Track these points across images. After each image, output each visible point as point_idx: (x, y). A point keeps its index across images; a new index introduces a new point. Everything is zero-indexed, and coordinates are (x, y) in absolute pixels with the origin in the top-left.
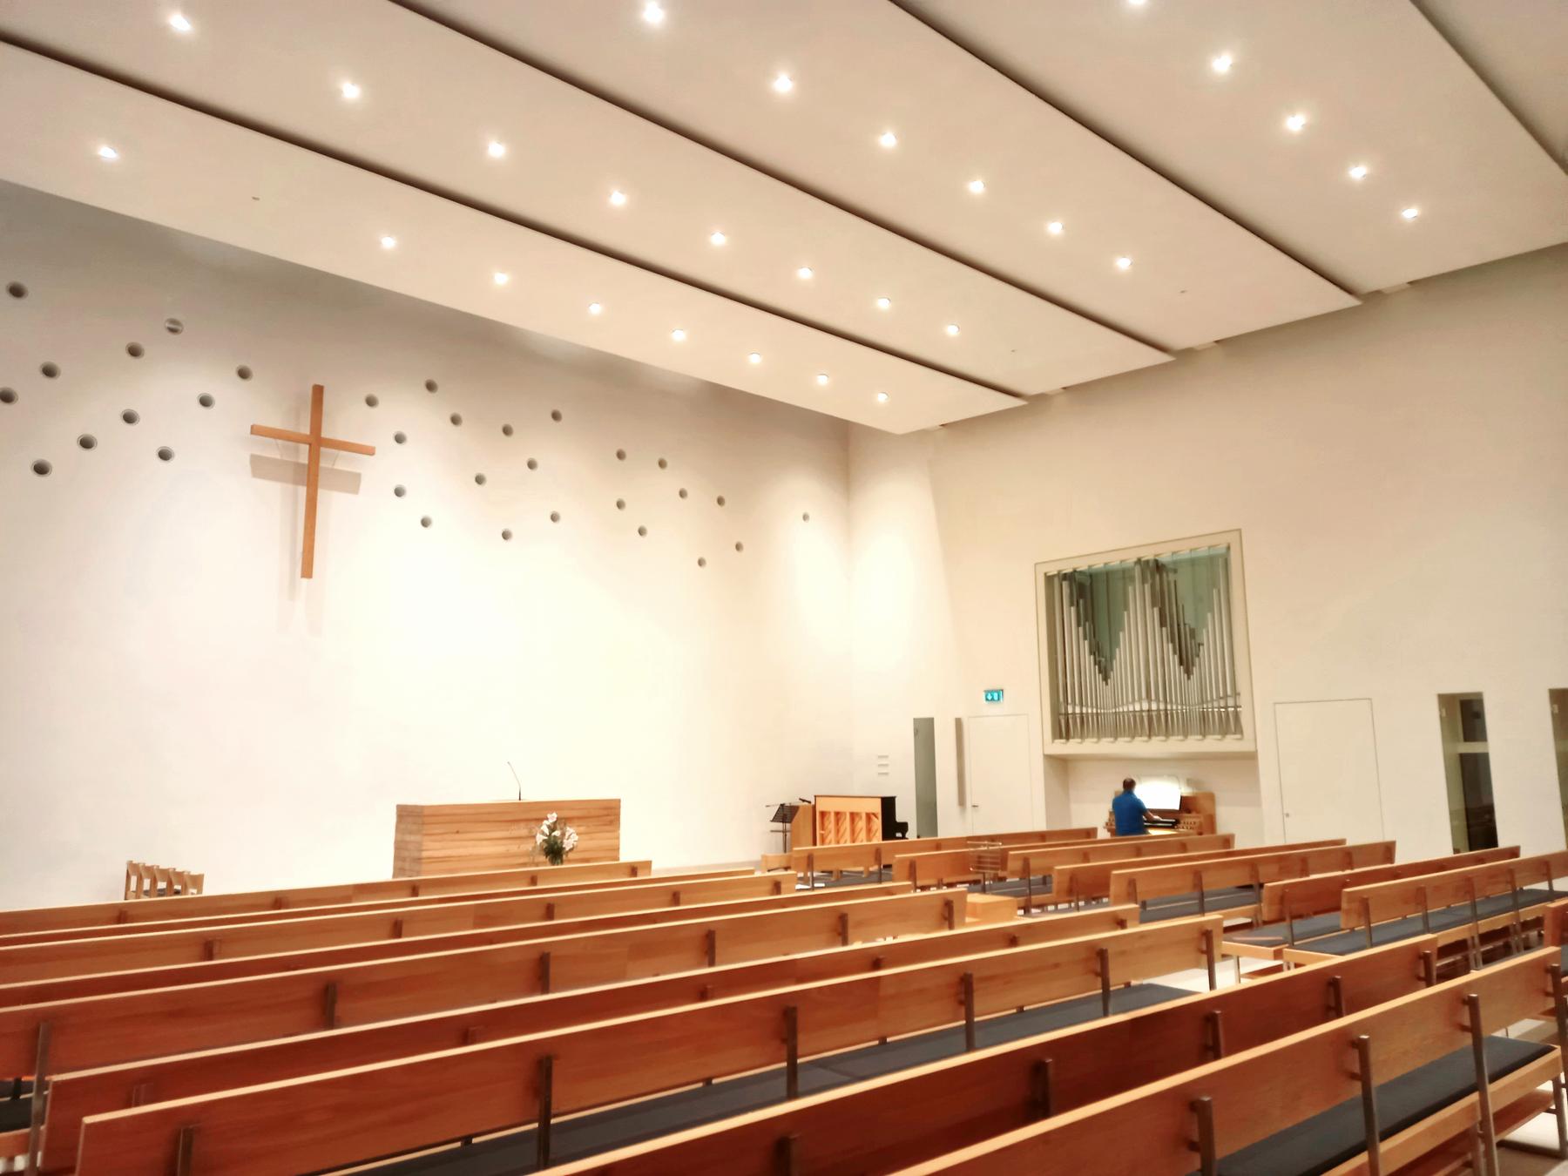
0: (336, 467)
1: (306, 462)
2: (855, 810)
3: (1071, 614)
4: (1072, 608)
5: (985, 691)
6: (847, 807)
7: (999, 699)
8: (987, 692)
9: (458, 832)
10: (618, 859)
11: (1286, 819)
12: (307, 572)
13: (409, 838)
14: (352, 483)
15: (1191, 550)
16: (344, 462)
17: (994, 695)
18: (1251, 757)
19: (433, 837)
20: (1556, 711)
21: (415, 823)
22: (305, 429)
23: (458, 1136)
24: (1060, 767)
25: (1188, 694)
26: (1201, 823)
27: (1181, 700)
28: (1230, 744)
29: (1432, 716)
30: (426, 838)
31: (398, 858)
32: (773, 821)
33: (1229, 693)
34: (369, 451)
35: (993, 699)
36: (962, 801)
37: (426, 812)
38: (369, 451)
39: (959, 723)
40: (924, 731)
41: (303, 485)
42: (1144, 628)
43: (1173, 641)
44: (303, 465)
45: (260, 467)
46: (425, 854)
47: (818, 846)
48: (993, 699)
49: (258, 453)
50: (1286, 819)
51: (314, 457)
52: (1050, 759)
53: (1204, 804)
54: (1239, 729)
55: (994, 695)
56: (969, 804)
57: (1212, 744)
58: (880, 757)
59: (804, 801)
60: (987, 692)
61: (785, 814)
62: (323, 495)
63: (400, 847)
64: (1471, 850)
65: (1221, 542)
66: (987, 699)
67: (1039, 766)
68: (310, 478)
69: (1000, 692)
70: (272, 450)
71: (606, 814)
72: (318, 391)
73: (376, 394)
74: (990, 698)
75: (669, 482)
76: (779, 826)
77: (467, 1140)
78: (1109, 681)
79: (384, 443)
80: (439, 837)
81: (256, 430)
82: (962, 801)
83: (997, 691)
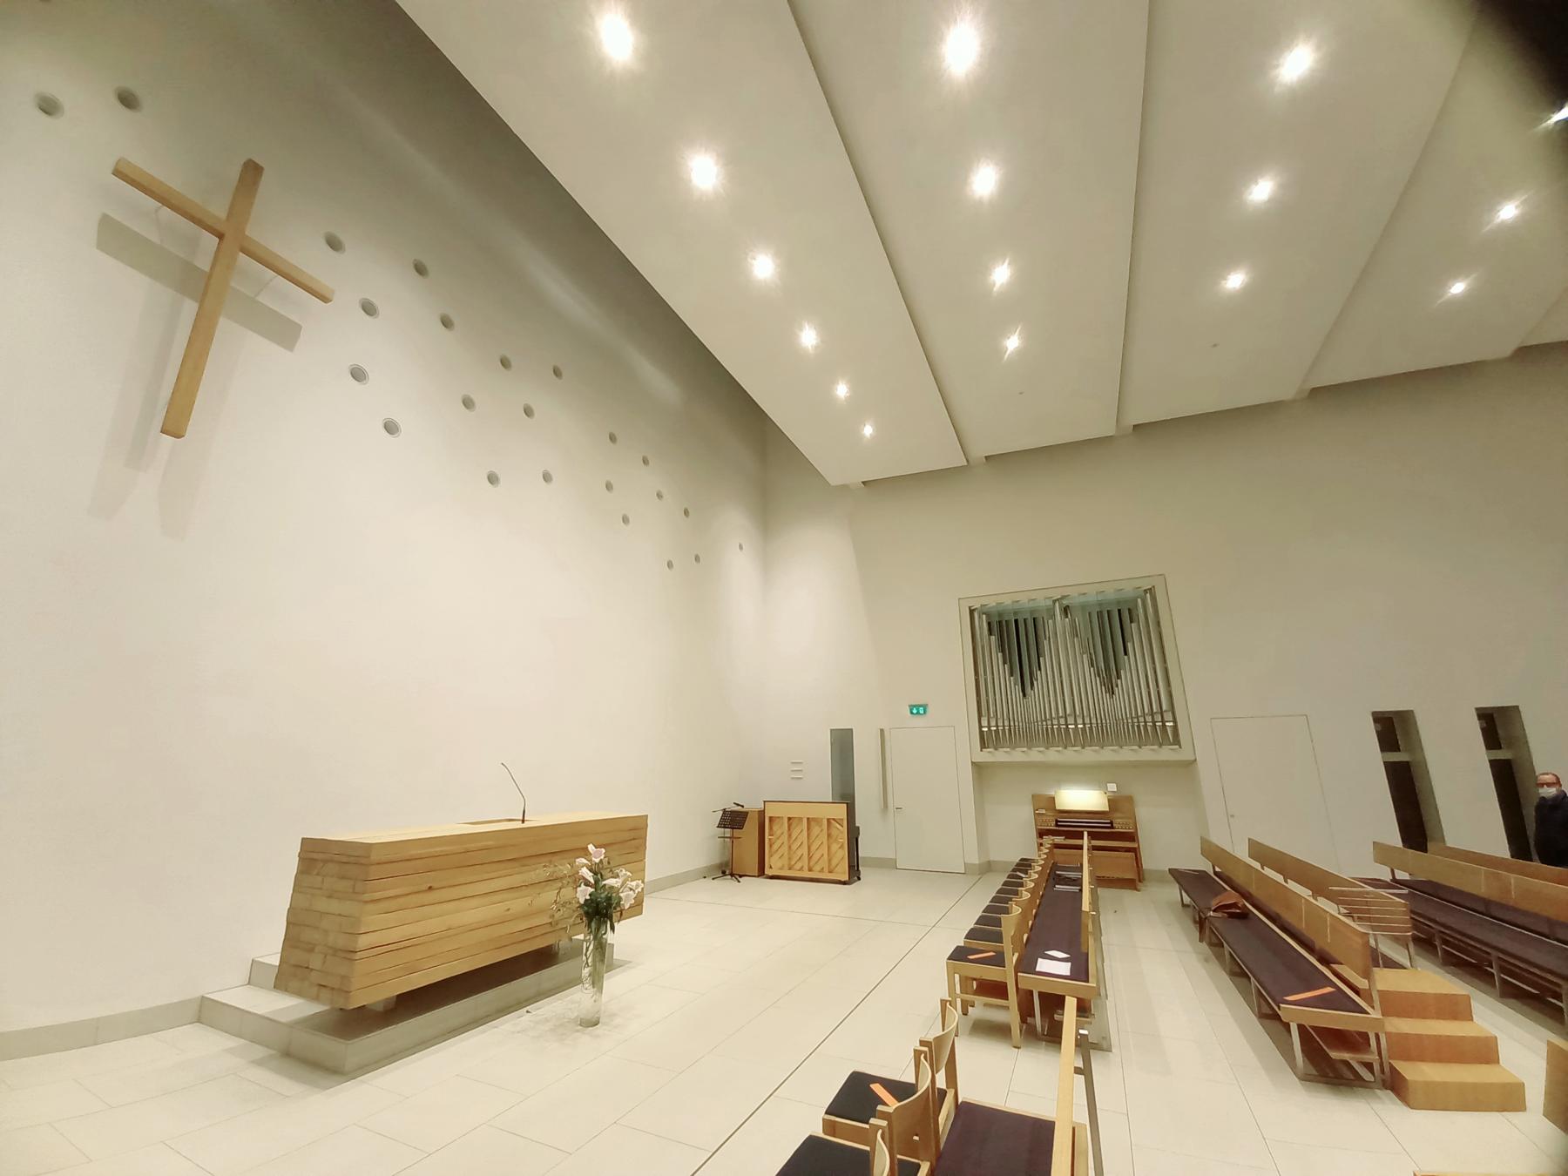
0: (260, 299)
1: (207, 269)
5: (910, 706)
6: (794, 811)
7: (925, 712)
8: (912, 707)
11: (1231, 819)
12: (174, 426)
13: (322, 904)
14: (285, 333)
15: (1097, 593)
16: (280, 296)
17: (918, 709)
21: (343, 878)
28: (1167, 753)
30: (370, 907)
31: (290, 941)
33: (1048, 717)
35: (918, 713)
37: (374, 857)
39: (882, 731)
40: (843, 744)
41: (196, 301)
42: (1159, 640)
44: (206, 272)
46: (363, 942)
48: (918, 713)
49: (112, 215)
50: (1231, 819)
52: (976, 766)
54: (1177, 741)
55: (918, 709)
57: (1148, 753)
59: (738, 805)
60: (912, 707)
61: (733, 820)
62: (226, 329)
63: (297, 922)
66: (912, 713)
67: (967, 773)
69: (925, 707)
74: (915, 711)
79: (347, 298)
83: (921, 706)
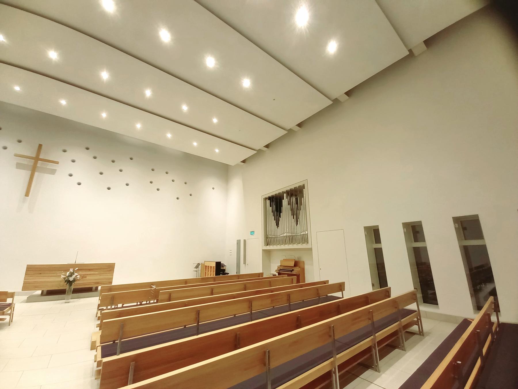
2: (210, 265)
3: (270, 209)
4: (271, 207)
9: (40, 274)
10: (111, 283)
12: (27, 194)
16: (50, 166)
18: (311, 249)
19: (29, 275)
20: (405, 231)
22: (34, 155)
23: (233, 314)
24: (267, 254)
25: (299, 231)
26: (299, 271)
27: (272, 234)
28: (304, 246)
29: (362, 236)
32: (195, 268)
34: (57, 163)
36: (245, 263)
38: (57, 163)
40: (239, 242)
43: (273, 212)
45: (19, 166)
47: (207, 277)
51: (35, 164)
52: (264, 251)
53: (301, 265)
56: (246, 264)
58: (230, 250)
62: (36, 174)
64: (381, 288)
65: (301, 184)
68: (34, 169)
70: (25, 162)
71: (110, 268)
72: (40, 146)
73: (66, 149)
75: (170, 177)
76: (196, 270)
77: (235, 315)
78: (278, 228)
80: (31, 275)
81: (16, 155)
82: (245, 263)
83: (253, 232)
